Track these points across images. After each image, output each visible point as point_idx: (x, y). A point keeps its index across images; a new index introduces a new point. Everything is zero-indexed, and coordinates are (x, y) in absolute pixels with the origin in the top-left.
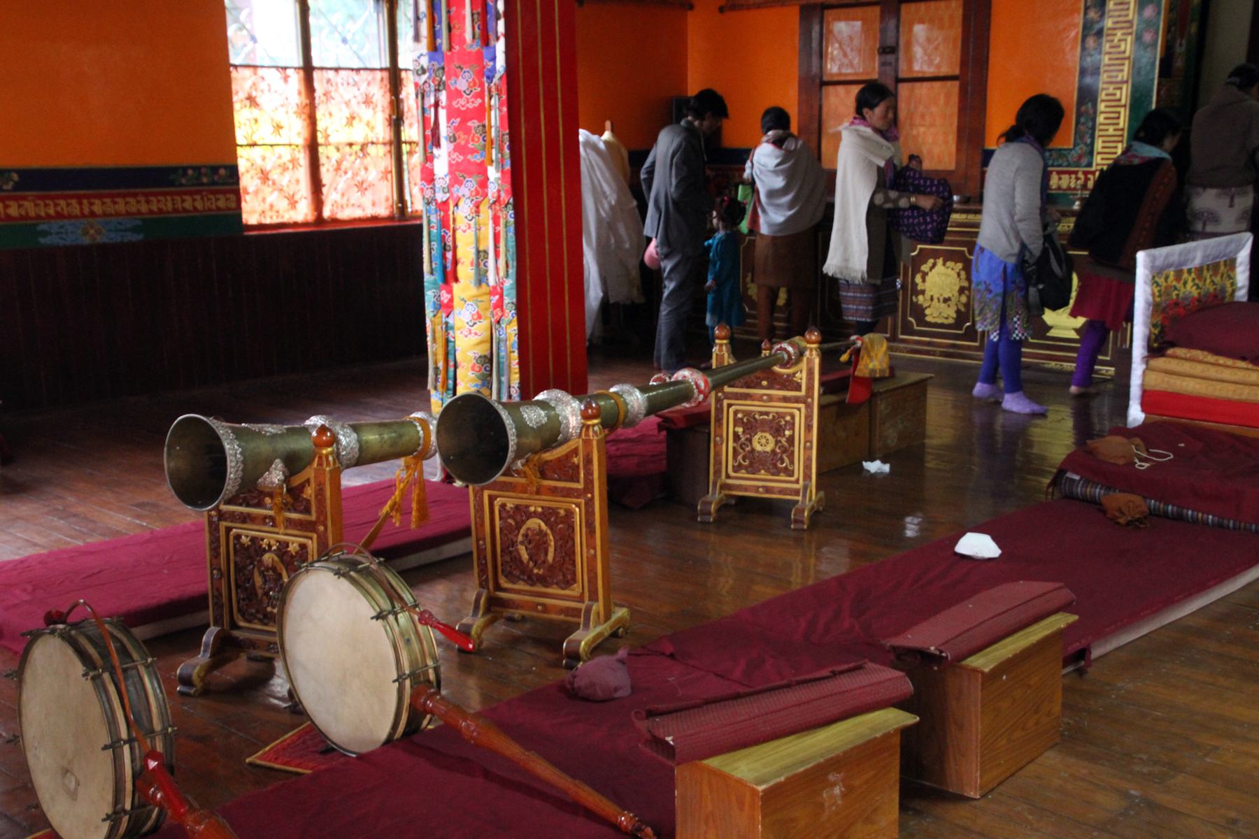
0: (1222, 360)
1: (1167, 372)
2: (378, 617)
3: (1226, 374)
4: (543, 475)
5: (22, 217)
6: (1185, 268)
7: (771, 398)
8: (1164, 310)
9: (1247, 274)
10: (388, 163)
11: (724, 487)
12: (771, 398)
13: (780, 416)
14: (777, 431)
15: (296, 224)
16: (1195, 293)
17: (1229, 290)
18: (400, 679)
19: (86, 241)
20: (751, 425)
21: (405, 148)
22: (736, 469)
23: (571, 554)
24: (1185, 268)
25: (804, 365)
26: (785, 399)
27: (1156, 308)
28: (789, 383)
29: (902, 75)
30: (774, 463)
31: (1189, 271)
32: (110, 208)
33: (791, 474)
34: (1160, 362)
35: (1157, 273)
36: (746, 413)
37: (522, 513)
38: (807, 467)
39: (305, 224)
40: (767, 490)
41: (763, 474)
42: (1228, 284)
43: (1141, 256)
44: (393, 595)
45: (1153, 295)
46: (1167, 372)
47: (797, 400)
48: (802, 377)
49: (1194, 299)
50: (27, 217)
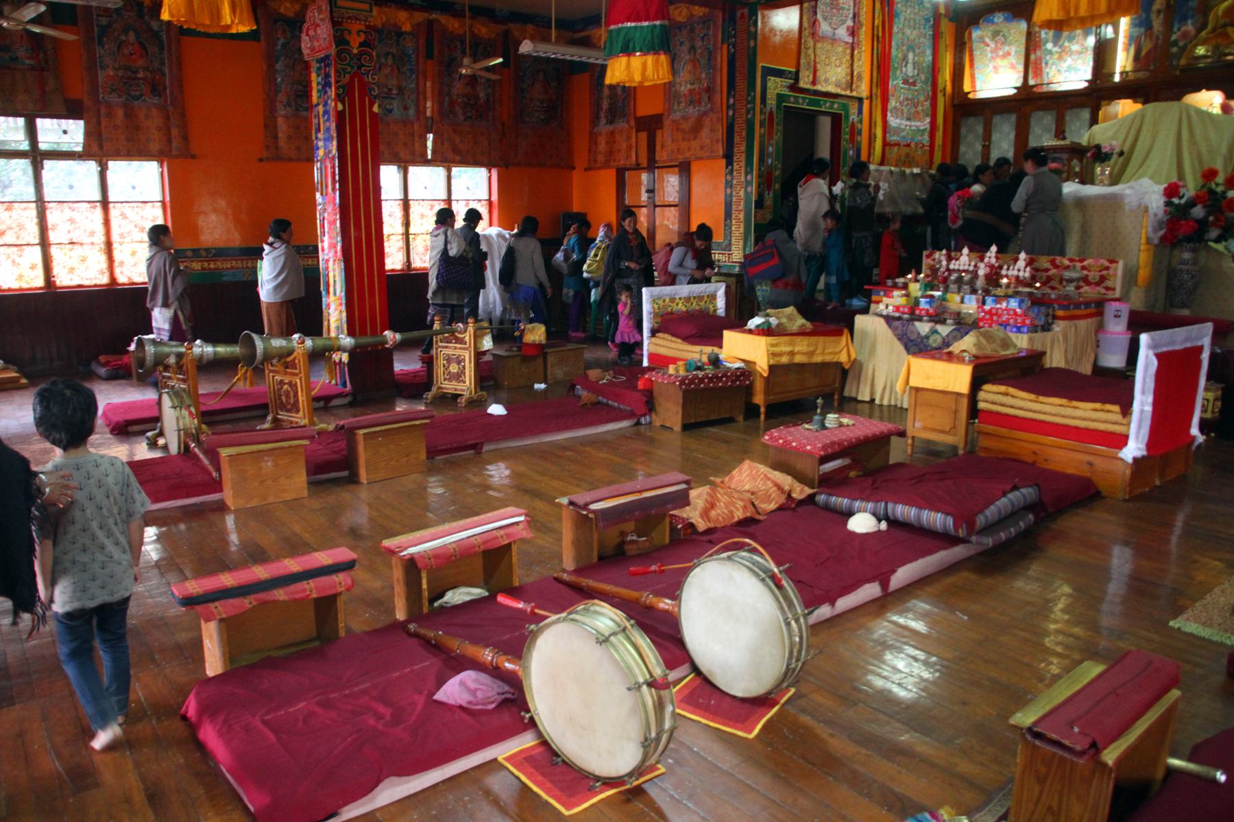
0: (674, 339)
1: (656, 345)
2: (172, 407)
3: (673, 345)
4: (287, 367)
5: (215, 269)
6: (677, 297)
7: (456, 348)
8: (662, 316)
9: (724, 302)
10: (401, 244)
11: (439, 388)
12: (456, 348)
13: (460, 356)
14: (459, 363)
15: (100, 286)
16: (684, 309)
17: (712, 309)
18: (179, 430)
19: (245, 279)
20: (449, 360)
21: (411, 237)
22: (445, 379)
23: (298, 401)
24: (677, 297)
25: (468, 334)
26: (461, 348)
27: (655, 315)
28: (461, 341)
29: (657, 203)
30: (458, 377)
31: (680, 299)
32: (240, 265)
33: (464, 382)
34: (653, 340)
35: (654, 301)
36: (448, 355)
37: (282, 382)
38: (470, 380)
39: (40, 288)
40: (456, 390)
41: (454, 383)
42: (711, 306)
43: (644, 290)
44: (182, 402)
45: (654, 308)
46: (656, 345)
47: (465, 349)
48: (467, 339)
49: (684, 312)
50: (218, 269)
